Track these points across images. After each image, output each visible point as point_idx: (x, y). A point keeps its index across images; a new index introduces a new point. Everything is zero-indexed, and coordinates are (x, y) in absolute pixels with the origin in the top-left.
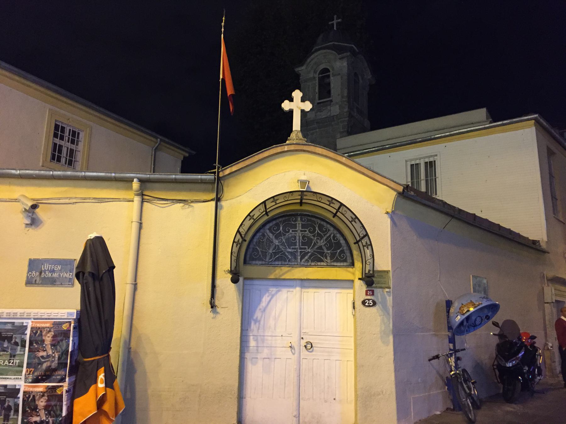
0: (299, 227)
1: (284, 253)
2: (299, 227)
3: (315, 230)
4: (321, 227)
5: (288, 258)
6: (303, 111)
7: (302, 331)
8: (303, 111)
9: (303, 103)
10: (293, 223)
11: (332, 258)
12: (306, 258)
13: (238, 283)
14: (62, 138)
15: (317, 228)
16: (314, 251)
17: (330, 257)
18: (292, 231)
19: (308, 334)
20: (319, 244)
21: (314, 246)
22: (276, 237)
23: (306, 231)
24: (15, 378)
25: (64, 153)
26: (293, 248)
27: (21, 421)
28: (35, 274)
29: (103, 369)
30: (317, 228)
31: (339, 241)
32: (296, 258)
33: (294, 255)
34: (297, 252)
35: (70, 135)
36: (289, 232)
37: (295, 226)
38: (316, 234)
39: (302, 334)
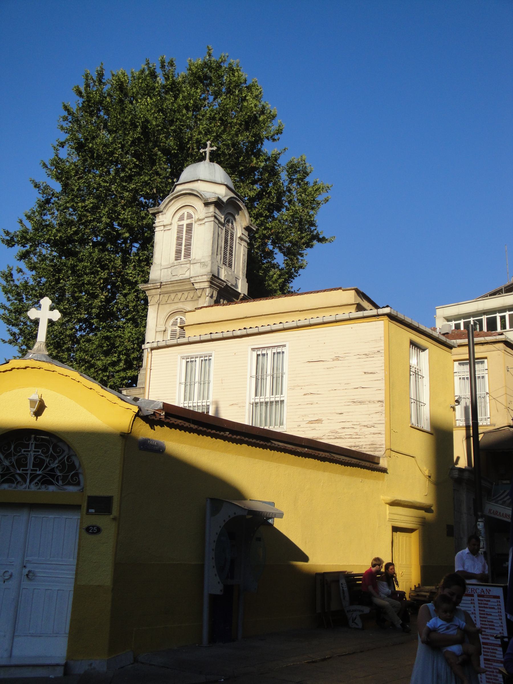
0: (32, 448)
1: (13, 476)
2: (32, 448)
3: (48, 450)
4: (55, 447)
5: (16, 479)
6: (50, 321)
8: (50, 321)
9: (51, 312)
10: (26, 442)
11: (63, 480)
12: (36, 481)
13: (161, 441)
15: (51, 449)
16: (46, 474)
18: (24, 451)
19: (32, 562)
20: (53, 466)
22: (6, 457)
23: (39, 452)
26: (23, 470)
27: (68, 646)
28: (36, 306)
29: (456, 466)
30: (51, 449)
31: (73, 463)
32: (25, 481)
33: (23, 477)
34: (27, 474)
36: (20, 451)
37: (27, 446)
38: (49, 455)
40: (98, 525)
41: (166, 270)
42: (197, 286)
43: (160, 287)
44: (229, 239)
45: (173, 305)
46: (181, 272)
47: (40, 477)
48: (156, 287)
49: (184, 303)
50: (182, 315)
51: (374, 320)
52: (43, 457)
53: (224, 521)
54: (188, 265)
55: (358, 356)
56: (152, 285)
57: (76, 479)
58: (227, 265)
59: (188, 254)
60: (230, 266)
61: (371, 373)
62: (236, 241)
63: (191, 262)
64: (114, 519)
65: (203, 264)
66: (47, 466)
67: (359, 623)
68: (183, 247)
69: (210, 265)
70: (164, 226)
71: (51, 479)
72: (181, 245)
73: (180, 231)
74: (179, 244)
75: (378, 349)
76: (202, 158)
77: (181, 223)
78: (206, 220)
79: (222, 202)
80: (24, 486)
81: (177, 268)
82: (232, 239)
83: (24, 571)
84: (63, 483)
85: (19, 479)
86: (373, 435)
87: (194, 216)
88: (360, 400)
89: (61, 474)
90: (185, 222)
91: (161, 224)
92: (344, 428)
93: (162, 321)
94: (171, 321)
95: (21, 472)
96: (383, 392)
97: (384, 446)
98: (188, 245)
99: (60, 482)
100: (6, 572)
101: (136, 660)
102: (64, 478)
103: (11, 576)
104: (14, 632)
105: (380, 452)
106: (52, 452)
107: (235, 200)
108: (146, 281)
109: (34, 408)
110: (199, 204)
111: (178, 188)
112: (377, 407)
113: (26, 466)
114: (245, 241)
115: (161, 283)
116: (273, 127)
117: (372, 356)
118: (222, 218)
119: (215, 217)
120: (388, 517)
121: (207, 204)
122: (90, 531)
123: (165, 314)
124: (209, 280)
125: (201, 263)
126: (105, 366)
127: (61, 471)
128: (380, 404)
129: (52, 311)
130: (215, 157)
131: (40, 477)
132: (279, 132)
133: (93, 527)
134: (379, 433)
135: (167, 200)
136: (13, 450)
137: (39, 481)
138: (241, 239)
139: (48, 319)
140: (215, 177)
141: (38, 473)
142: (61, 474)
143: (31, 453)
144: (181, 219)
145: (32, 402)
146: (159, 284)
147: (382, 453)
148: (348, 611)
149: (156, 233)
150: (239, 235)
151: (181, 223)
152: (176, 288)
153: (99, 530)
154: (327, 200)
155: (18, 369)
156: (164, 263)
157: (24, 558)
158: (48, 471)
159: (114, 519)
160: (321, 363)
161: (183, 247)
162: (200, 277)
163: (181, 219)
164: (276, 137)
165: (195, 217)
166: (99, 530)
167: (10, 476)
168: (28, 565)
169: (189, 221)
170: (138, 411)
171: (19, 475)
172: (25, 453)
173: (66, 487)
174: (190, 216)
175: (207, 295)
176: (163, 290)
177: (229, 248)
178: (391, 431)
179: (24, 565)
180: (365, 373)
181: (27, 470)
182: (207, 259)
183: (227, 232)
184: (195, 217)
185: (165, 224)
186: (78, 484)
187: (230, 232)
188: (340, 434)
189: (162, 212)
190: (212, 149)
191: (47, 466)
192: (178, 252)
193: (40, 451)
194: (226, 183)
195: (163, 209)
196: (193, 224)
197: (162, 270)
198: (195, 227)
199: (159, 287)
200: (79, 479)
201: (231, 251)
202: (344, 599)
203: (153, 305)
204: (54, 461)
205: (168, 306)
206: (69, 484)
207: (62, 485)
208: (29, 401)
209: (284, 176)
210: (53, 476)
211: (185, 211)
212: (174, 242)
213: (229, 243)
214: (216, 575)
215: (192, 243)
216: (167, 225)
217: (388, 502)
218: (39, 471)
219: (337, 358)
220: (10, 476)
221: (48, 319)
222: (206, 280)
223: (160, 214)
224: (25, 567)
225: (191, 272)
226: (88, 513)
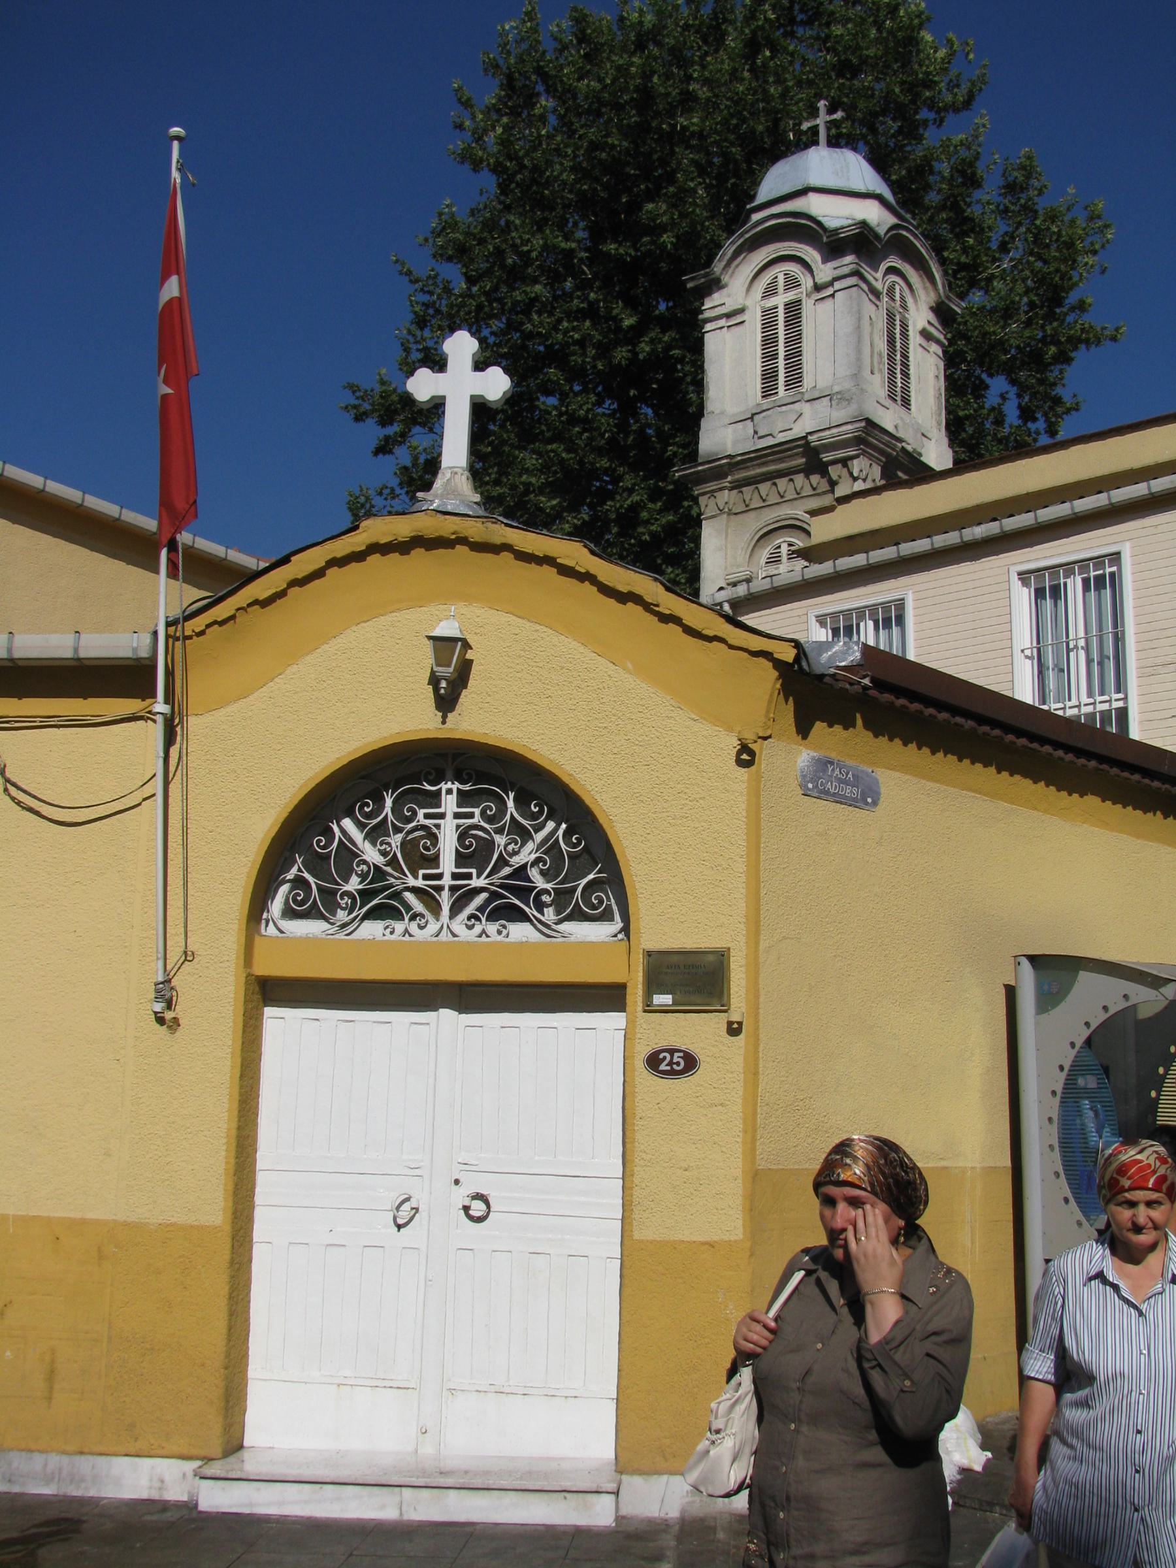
0: (449, 804)
1: (397, 895)
2: (449, 804)
5: (409, 908)
12: (470, 909)
15: (510, 804)
16: (501, 886)
18: (427, 816)
20: (517, 861)
23: (471, 815)
26: (426, 877)
30: (510, 804)
44: (898, 336)
47: (484, 895)
49: (795, 502)
50: (792, 534)
57: (601, 902)
58: (899, 402)
59: (795, 378)
60: (906, 403)
62: (915, 339)
66: (502, 862)
68: (781, 363)
71: (517, 902)
72: (775, 356)
73: (769, 323)
74: (769, 356)
76: (809, 140)
79: (877, 236)
81: (769, 416)
84: (558, 913)
85: (417, 906)
89: (549, 886)
90: (780, 300)
94: (764, 554)
95: (420, 883)
98: (795, 356)
102: (562, 897)
106: (516, 815)
107: (904, 233)
109: (449, 666)
113: (434, 861)
114: (938, 342)
118: (876, 280)
122: (663, 1067)
123: (747, 536)
125: (830, 396)
129: (482, 370)
131: (484, 895)
133: (672, 1051)
136: (390, 814)
137: (481, 909)
138: (925, 334)
139: (472, 397)
140: (848, 179)
141: (476, 882)
142: (549, 886)
144: (771, 291)
150: (920, 327)
152: (772, 468)
153: (691, 1063)
161: (781, 363)
163: (771, 291)
166: (691, 1063)
167: (388, 897)
169: (791, 296)
172: (428, 822)
173: (566, 927)
183: (891, 316)
187: (898, 318)
192: (769, 377)
193: (477, 811)
194: (878, 191)
195: (721, 273)
196: (804, 302)
198: (808, 307)
201: (905, 366)
203: (713, 517)
205: (752, 514)
206: (578, 915)
208: (429, 645)
210: (524, 892)
211: (779, 271)
213: (898, 345)
214: (1066, 1200)
218: (479, 876)
220: (388, 897)
221: (472, 397)
226: (649, 1009)
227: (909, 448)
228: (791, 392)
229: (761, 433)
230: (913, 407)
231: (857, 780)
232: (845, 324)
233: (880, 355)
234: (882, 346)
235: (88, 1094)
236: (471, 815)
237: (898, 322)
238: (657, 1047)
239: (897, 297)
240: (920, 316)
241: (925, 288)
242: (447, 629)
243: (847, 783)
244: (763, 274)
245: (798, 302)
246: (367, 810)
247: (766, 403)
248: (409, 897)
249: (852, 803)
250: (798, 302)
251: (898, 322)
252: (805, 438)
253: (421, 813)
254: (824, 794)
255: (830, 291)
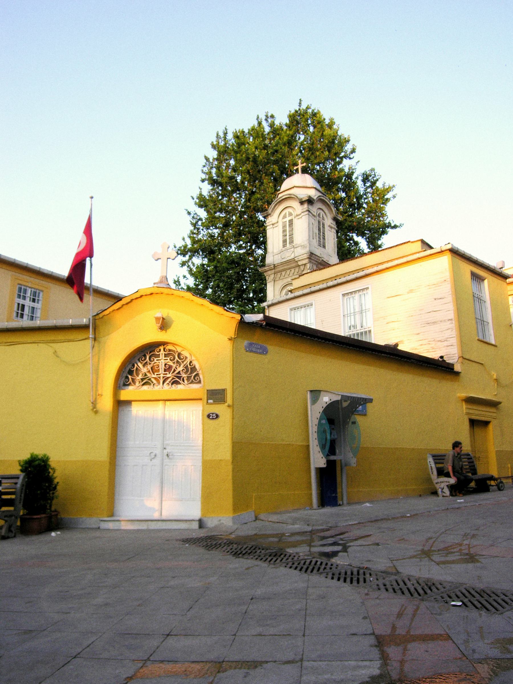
0: (162, 357)
1: (150, 379)
2: (162, 357)
3: (174, 359)
5: (153, 382)
7: (165, 443)
12: (167, 382)
14: (24, 298)
16: (175, 376)
17: (187, 380)
18: (157, 360)
21: (173, 372)
23: (167, 359)
24: (332, 567)
25: (477, 415)
26: (157, 375)
32: (159, 383)
35: (21, 290)
37: (158, 356)
39: (165, 445)
40: (218, 413)
41: (277, 255)
42: (300, 263)
43: (274, 268)
45: (284, 279)
46: (288, 255)
48: (271, 268)
51: (441, 255)
52: (171, 363)
53: (323, 407)
54: (292, 249)
55: (429, 287)
56: (268, 268)
59: (291, 242)
60: (324, 247)
61: (440, 299)
63: (295, 247)
64: (229, 406)
65: (303, 247)
66: (175, 371)
67: (447, 492)
69: (308, 246)
70: (273, 224)
72: (286, 236)
73: (284, 226)
75: (444, 279)
77: (284, 220)
78: (302, 214)
80: (159, 387)
82: (324, 227)
83: (164, 452)
84: (188, 382)
86: (446, 348)
87: (293, 213)
88: (433, 321)
90: (288, 219)
91: (271, 223)
92: (421, 345)
93: (277, 292)
95: (155, 376)
96: (452, 312)
97: (457, 355)
98: (291, 235)
99: (186, 381)
100: (151, 453)
101: (256, 519)
103: (155, 455)
104: (162, 498)
105: (453, 360)
108: (264, 266)
110: (295, 204)
111: (280, 196)
112: (448, 325)
114: (334, 228)
115: (274, 265)
116: (348, 148)
117: (440, 285)
119: (309, 211)
120: (465, 411)
121: (302, 203)
124: (308, 257)
125: (301, 246)
126: (204, 276)
127: (186, 373)
128: (450, 322)
130: (305, 171)
131: (170, 379)
132: (353, 151)
133: (213, 414)
134: (452, 345)
135: (273, 205)
141: (168, 376)
143: (162, 360)
144: (285, 217)
145: (157, 319)
146: (273, 266)
147: (456, 360)
148: (436, 483)
149: (267, 231)
151: (284, 220)
152: (286, 267)
153: (217, 416)
154: (394, 197)
155: (146, 295)
156: (276, 251)
157: (164, 442)
158: (177, 374)
159: (229, 406)
160: (398, 297)
161: (288, 237)
162: (302, 256)
164: (351, 156)
165: (294, 214)
168: (167, 447)
169: (290, 218)
170: (241, 319)
171: (155, 378)
174: (290, 214)
175: (308, 268)
176: (277, 270)
177: (322, 234)
178: (462, 343)
179: (165, 447)
180: (435, 299)
181: (160, 374)
182: (306, 243)
183: (319, 222)
184: (294, 214)
185: (273, 223)
186: (200, 382)
188: (419, 350)
189: (270, 214)
190: (303, 165)
191: (175, 371)
192: (285, 241)
194: (315, 186)
197: (275, 256)
198: (295, 221)
199: (273, 268)
200: (200, 378)
202: (432, 474)
204: (180, 366)
205: (281, 281)
206: (192, 382)
207: (187, 384)
209: (360, 183)
210: (179, 378)
211: (287, 211)
212: (281, 234)
213: (322, 230)
215: (294, 233)
216: (274, 224)
217: (463, 399)
219: (411, 291)
222: (306, 257)
223: (269, 216)
224: (165, 448)
225: (296, 253)
227: (325, 260)
228: (291, 246)
229: (282, 258)
230: (326, 248)
231: (261, 347)
232: (306, 225)
233: (316, 234)
234: (317, 232)
235: (429, 574)
236: (167, 359)
237: (321, 224)
238: (210, 413)
239: (321, 216)
240: (329, 222)
241: (330, 213)
242: (159, 315)
243: (258, 348)
244: (282, 212)
245: (292, 220)
246: (143, 359)
247: (284, 249)
248: (153, 380)
249: (260, 353)
250: (292, 220)
251: (321, 224)
252: (294, 259)
253: (156, 359)
254: (251, 351)
255: (301, 216)
